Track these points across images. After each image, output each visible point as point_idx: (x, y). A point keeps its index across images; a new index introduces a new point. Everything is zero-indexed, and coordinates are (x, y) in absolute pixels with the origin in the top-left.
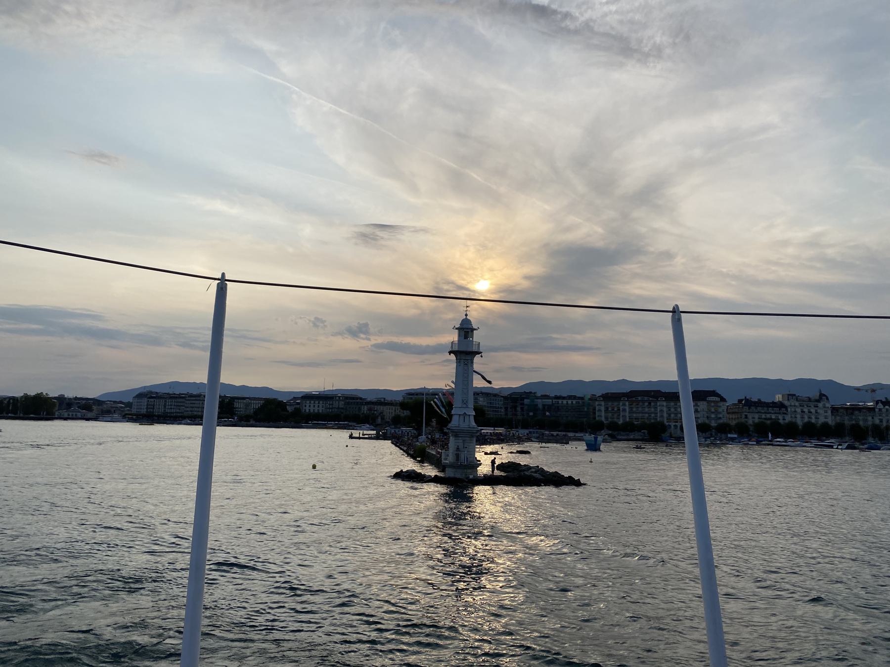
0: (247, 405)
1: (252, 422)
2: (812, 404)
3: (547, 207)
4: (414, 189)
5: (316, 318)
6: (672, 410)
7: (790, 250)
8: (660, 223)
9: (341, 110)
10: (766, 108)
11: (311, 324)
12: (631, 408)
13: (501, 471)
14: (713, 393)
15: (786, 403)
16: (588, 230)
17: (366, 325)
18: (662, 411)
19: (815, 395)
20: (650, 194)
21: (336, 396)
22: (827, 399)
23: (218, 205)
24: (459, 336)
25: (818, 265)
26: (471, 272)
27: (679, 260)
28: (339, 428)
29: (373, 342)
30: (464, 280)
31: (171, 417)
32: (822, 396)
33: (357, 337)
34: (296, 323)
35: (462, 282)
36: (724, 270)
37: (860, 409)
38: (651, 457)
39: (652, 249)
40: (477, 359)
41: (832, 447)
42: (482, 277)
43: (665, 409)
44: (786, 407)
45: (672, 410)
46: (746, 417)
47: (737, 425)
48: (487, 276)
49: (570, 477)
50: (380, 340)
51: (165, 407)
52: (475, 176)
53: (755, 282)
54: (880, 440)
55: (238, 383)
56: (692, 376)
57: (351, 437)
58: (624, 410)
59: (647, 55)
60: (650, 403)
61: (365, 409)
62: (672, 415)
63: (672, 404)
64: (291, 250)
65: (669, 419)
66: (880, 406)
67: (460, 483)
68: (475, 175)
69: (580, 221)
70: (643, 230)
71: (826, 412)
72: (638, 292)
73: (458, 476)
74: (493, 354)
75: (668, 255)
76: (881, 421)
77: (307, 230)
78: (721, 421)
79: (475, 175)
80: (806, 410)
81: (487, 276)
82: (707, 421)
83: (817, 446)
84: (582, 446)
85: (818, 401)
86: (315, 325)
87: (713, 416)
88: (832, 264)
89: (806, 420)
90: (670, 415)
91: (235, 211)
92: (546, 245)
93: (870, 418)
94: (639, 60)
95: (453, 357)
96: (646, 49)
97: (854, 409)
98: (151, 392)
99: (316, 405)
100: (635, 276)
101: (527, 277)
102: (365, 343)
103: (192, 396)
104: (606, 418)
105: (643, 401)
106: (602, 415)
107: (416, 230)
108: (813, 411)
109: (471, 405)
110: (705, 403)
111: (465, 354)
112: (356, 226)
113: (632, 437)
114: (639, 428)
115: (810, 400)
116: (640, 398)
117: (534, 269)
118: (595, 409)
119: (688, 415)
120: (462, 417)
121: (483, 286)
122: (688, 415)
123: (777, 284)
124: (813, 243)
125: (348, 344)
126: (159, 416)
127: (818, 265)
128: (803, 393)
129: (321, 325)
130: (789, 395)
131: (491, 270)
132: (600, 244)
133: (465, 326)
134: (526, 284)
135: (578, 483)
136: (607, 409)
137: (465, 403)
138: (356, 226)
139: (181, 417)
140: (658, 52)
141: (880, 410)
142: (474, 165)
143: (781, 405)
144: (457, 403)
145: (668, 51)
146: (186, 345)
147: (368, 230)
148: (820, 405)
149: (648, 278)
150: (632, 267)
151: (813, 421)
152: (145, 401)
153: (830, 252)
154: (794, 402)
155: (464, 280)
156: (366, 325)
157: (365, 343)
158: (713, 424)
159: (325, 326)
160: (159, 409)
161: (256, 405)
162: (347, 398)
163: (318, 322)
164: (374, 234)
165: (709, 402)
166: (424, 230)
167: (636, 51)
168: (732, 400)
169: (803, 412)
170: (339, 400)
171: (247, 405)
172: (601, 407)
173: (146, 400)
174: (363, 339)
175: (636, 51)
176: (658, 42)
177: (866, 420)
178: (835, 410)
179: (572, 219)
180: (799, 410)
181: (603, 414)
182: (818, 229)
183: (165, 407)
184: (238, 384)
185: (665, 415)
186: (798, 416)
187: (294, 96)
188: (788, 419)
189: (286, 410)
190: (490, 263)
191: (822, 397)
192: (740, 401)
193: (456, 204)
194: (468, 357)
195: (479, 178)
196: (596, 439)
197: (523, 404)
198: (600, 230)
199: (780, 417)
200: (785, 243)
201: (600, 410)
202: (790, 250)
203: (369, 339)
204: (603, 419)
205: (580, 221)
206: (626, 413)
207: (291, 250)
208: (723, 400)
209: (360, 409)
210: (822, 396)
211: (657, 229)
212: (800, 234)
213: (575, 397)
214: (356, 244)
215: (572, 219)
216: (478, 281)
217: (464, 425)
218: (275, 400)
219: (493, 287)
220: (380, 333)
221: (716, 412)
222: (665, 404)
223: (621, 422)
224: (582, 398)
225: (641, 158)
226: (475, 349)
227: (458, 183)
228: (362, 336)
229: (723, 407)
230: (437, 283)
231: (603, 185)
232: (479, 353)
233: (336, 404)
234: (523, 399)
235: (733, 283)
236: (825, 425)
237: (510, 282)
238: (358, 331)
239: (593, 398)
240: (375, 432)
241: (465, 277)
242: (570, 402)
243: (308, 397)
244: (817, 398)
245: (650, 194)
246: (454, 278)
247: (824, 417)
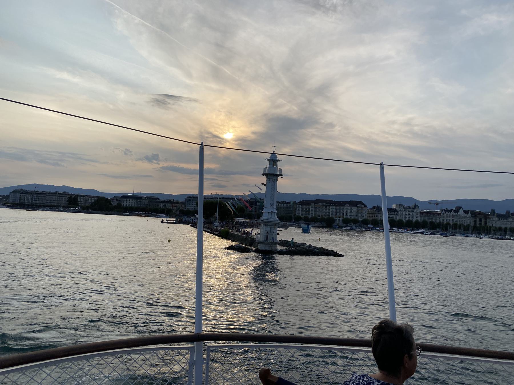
0: (86, 201)
1: (90, 211)
2: (411, 210)
3: (267, 93)
4: (189, 75)
5: (126, 149)
6: (338, 211)
7: (396, 127)
8: (328, 107)
9: (147, 24)
10: (391, 47)
11: (123, 153)
12: (316, 209)
13: (283, 246)
14: (360, 203)
15: (398, 209)
16: (290, 109)
17: (157, 155)
18: (332, 211)
19: (412, 205)
20: (323, 90)
21: (143, 197)
22: (418, 208)
23: (65, 76)
24: (270, 164)
25: (409, 135)
26: (222, 127)
27: (337, 128)
28: (145, 216)
29: (161, 165)
30: (217, 132)
31: (36, 206)
32: (416, 206)
33: (153, 162)
34: (113, 152)
35: (216, 133)
36: (361, 135)
37: (434, 214)
38: (347, 237)
39: (323, 121)
40: (279, 178)
41: (423, 233)
42: (228, 131)
43: (334, 210)
44: (398, 212)
45: (338, 211)
46: (377, 216)
47: (373, 220)
48: (231, 130)
49: (332, 251)
50: (166, 165)
51: (32, 199)
52: (226, 71)
53: (377, 143)
54: (334, 222)
55: (75, 187)
56: (388, 194)
57: (162, 222)
58: (312, 210)
59: (328, 9)
60: (326, 207)
61: (161, 205)
62: (338, 214)
63: (338, 208)
64: (111, 107)
65: (336, 216)
66: (444, 212)
67: (267, 252)
68: (226, 70)
69: (285, 102)
70: (319, 110)
71: (417, 215)
72: (314, 145)
73: (267, 249)
74: (232, 176)
75: (331, 125)
76: (443, 220)
77: (123, 95)
78: (364, 218)
79: (226, 70)
80: (407, 213)
81: (231, 130)
82: (356, 218)
83: (415, 233)
84: (301, 230)
85: (414, 209)
86: (125, 154)
87: (360, 215)
88: (416, 135)
89: (407, 219)
90: (336, 214)
91: (76, 80)
92: (265, 115)
93: (438, 218)
94: (324, 12)
95: (265, 178)
96: (328, 6)
97: (431, 213)
98: (22, 190)
99: (128, 202)
100: (313, 135)
101: (254, 133)
102: (156, 166)
103: (50, 193)
104: (302, 214)
105: (323, 206)
106: (299, 212)
107: (191, 100)
108: (411, 214)
109: (275, 207)
110: (356, 208)
111: (272, 176)
112: (153, 94)
113: (316, 225)
114: (321, 220)
115: (410, 208)
116: (321, 204)
117: (258, 128)
118: (296, 209)
119: (385, 217)
120: (270, 214)
121: (229, 135)
122: (385, 217)
123: (388, 144)
124: (408, 123)
125: (146, 166)
126: (28, 205)
127: (409, 135)
128: (407, 205)
129: (129, 153)
130: (399, 205)
131: (234, 127)
132: (295, 116)
133: (273, 159)
134: (253, 137)
135: (343, 256)
136: (302, 210)
137: (272, 205)
138: (153, 94)
139: (44, 206)
140: (334, 8)
141: (444, 214)
142: (223, 65)
143: (439, 214)
144: (266, 205)
145: (339, 8)
146: (42, 161)
147: (161, 98)
148: (415, 211)
149: (320, 137)
150: (311, 131)
151: (411, 219)
152: (18, 195)
153: (416, 129)
154: (402, 209)
155: (217, 132)
156: (157, 155)
157: (156, 166)
158: (360, 219)
159: (132, 154)
160: (28, 199)
161: (92, 200)
162: (150, 198)
163: (127, 152)
164: (163, 100)
165: (358, 207)
166: (195, 100)
167: (322, 6)
168: (370, 206)
169: (406, 214)
170: (145, 199)
171: (86, 201)
172: (299, 208)
173: (19, 195)
174: (155, 163)
175: (322, 6)
176: (335, 2)
177: (436, 220)
178: (422, 214)
179: (281, 101)
180: (404, 213)
181: (300, 212)
182: (410, 116)
183: (32, 199)
184: (75, 187)
185: (334, 214)
186: (404, 216)
187: (117, 11)
188: (398, 218)
189: (111, 204)
190: (233, 123)
191: (416, 206)
192: (374, 207)
193: (214, 86)
194: (275, 178)
195: (229, 72)
196: (308, 227)
197: (256, 205)
198: (296, 108)
199: (394, 217)
200: (394, 122)
201: (299, 210)
202: (396, 127)
203: (159, 164)
204: (300, 215)
205: (285, 102)
206: (312, 212)
207: (111, 107)
208: (365, 206)
209: (158, 205)
210: (416, 206)
211: (328, 111)
212: (401, 118)
213: (285, 202)
214: (153, 106)
215: (281, 101)
216: (226, 133)
217: (271, 219)
218: (104, 197)
219: (234, 137)
220: (166, 160)
221: (361, 213)
222: (334, 207)
223: (310, 217)
224: (289, 203)
225: (321, 68)
226: (278, 173)
227: (216, 75)
228: (155, 161)
229: (365, 210)
230: (201, 133)
231: (298, 83)
232: (281, 175)
233: (143, 202)
234: (256, 202)
235: (365, 143)
236: (417, 222)
237: (243, 135)
238: (152, 158)
239: (295, 203)
240: (175, 219)
241: (218, 130)
242: (282, 205)
243: (125, 197)
244: (414, 207)
245: (323, 90)
246: (212, 130)
247: (416, 218)
